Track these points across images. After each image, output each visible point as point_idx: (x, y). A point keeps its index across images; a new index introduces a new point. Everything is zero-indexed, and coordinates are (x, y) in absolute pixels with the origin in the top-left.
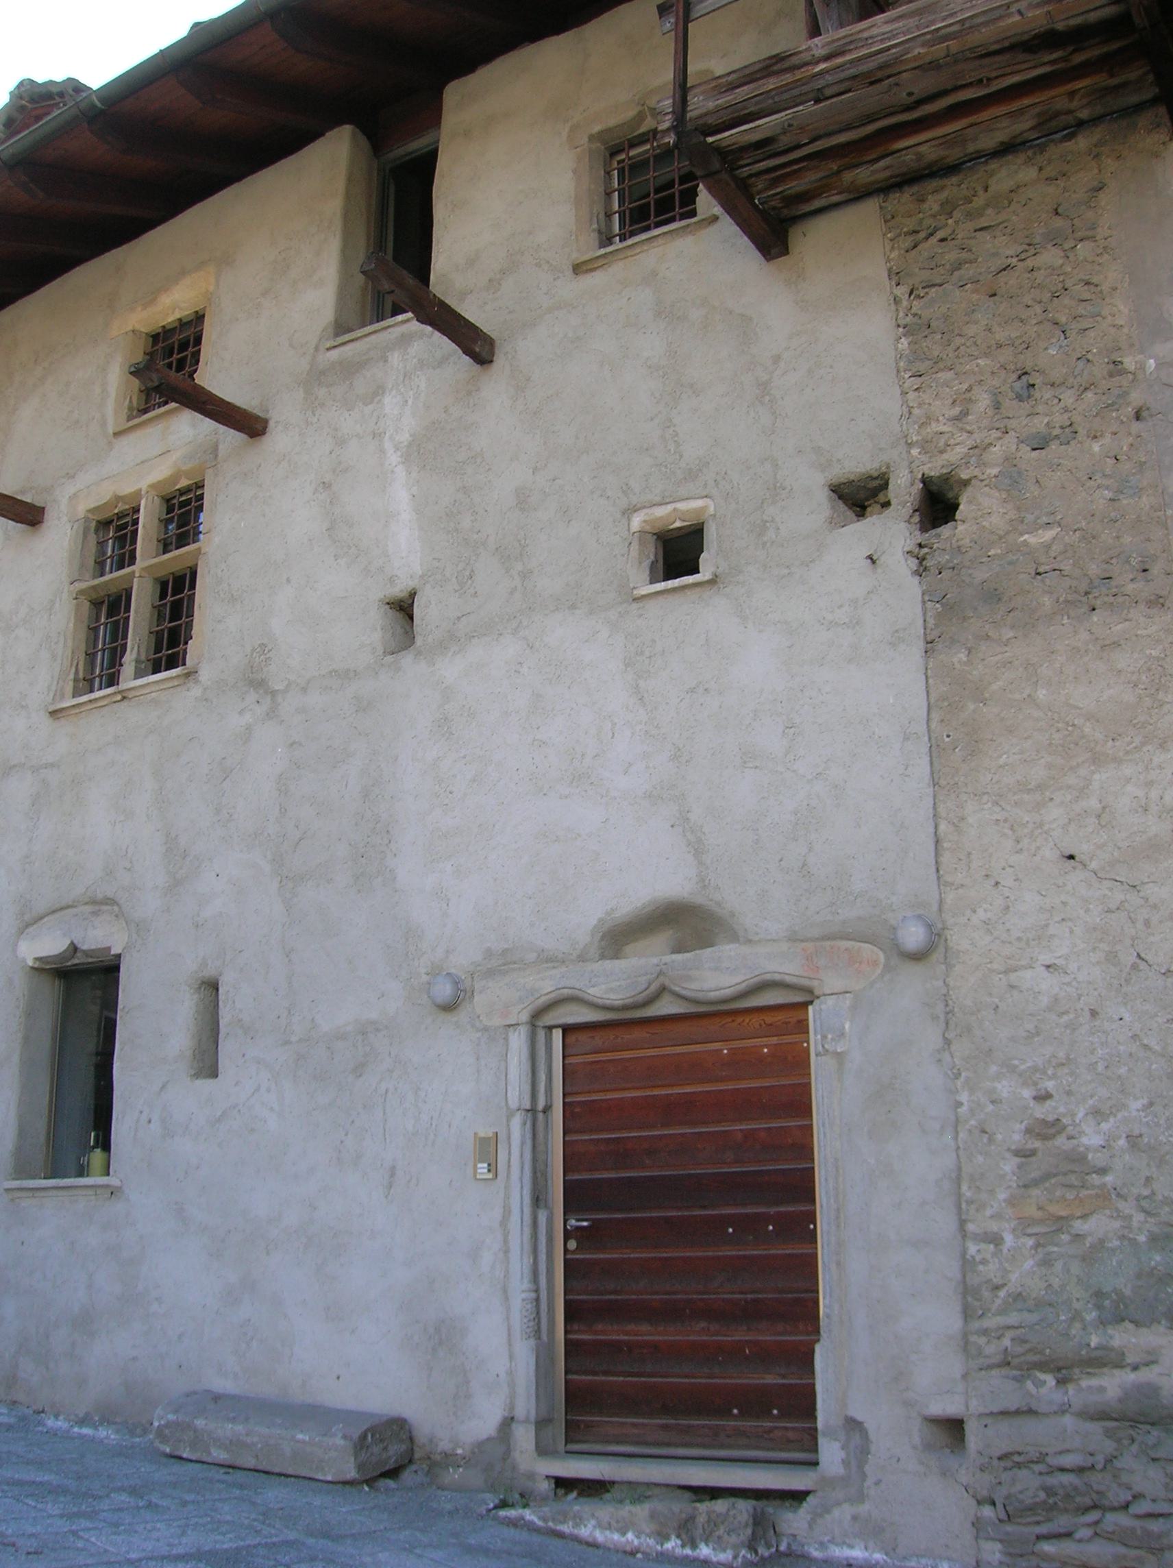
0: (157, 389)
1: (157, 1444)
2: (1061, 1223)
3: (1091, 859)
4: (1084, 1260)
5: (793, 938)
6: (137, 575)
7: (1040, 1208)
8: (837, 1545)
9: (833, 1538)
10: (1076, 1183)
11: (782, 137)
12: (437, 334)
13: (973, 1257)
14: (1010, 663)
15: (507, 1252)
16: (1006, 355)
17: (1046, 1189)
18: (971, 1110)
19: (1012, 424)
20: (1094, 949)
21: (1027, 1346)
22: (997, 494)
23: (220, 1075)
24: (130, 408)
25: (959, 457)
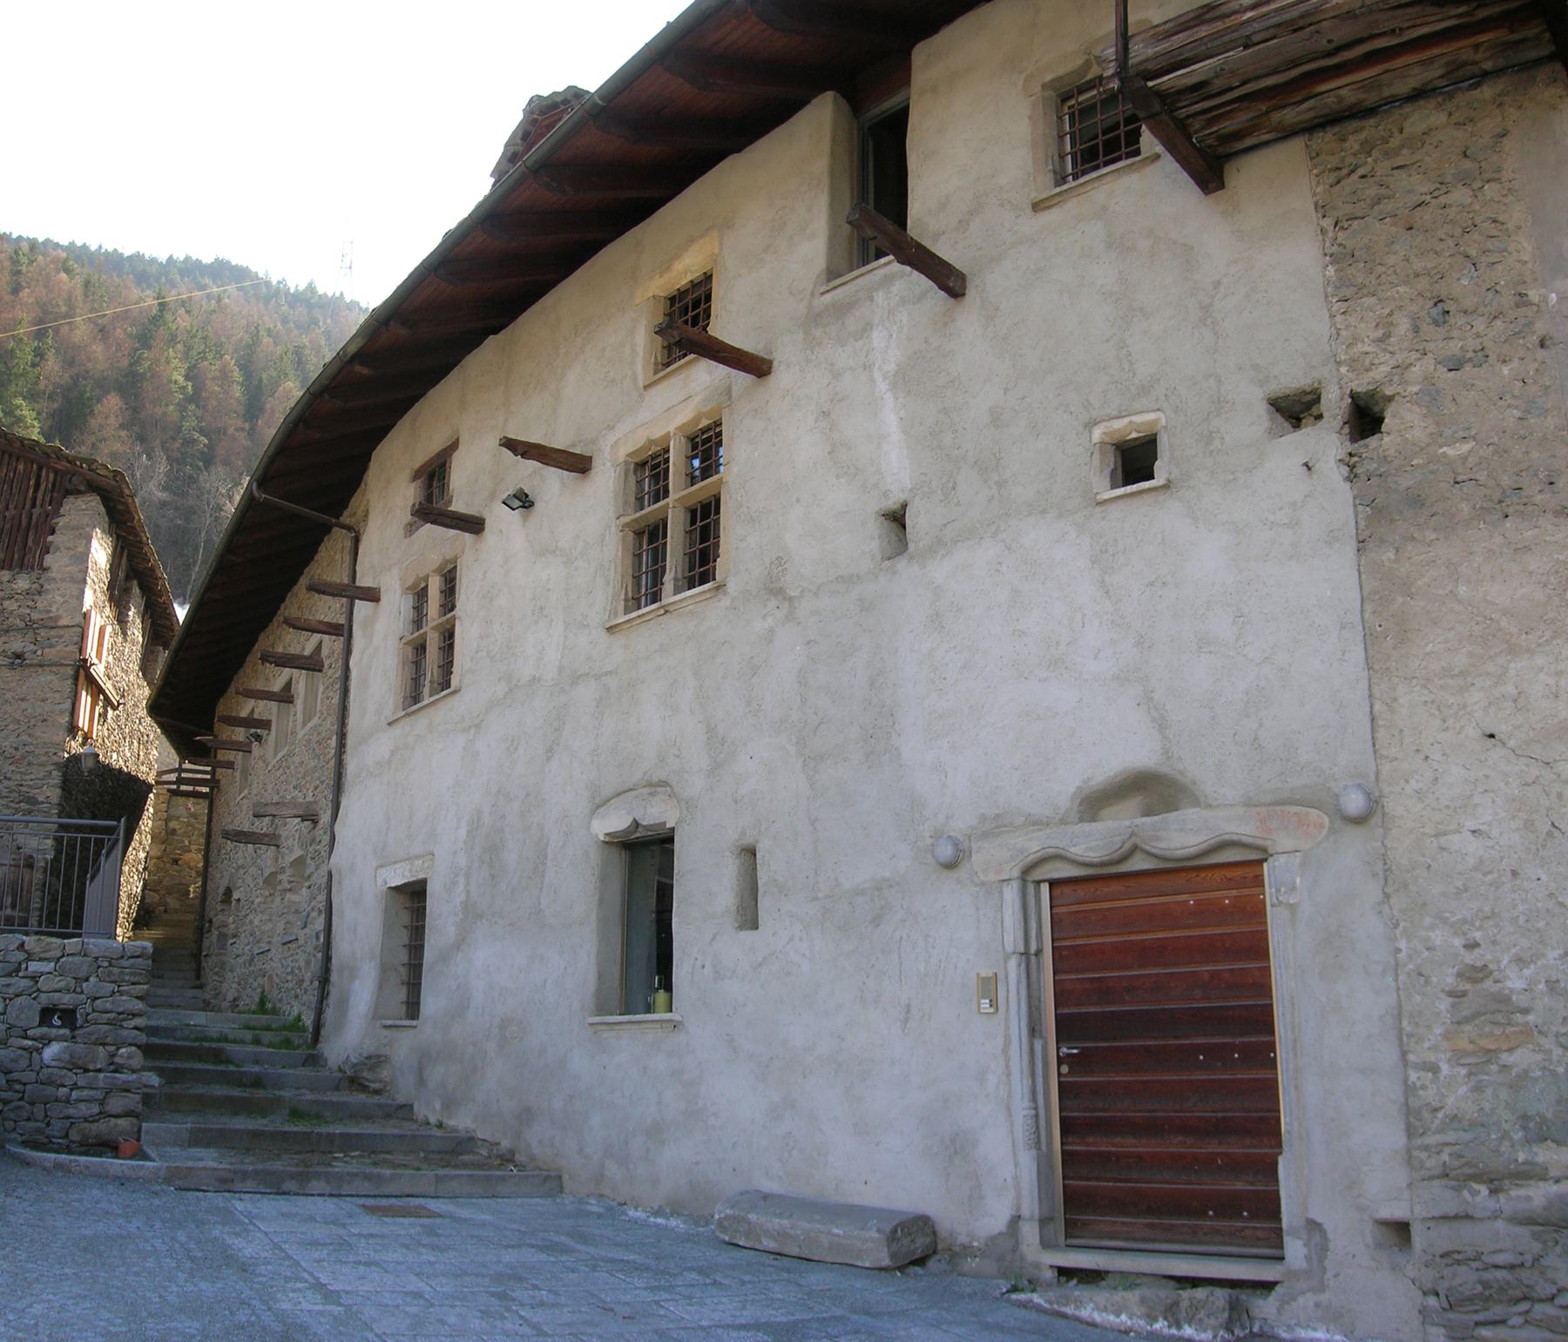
0: (679, 344)
1: (718, 1233)
2: (1490, 1055)
3: (1509, 738)
4: (1511, 1087)
5: (1248, 803)
7: (1471, 1042)
8: (1303, 1328)
9: (1299, 1322)
10: (1503, 1021)
11: (1216, 81)
12: (916, 273)
13: (1414, 1083)
14: (1433, 561)
15: (1009, 1075)
16: (1423, 284)
17: (1476, 1026)
18: (1410, 957)
19: (1430, 346)
20: (1514, 817)
21: (1463, 1160)
22: (1418, 410)
24: (656, 364)
25: (1383, 375)
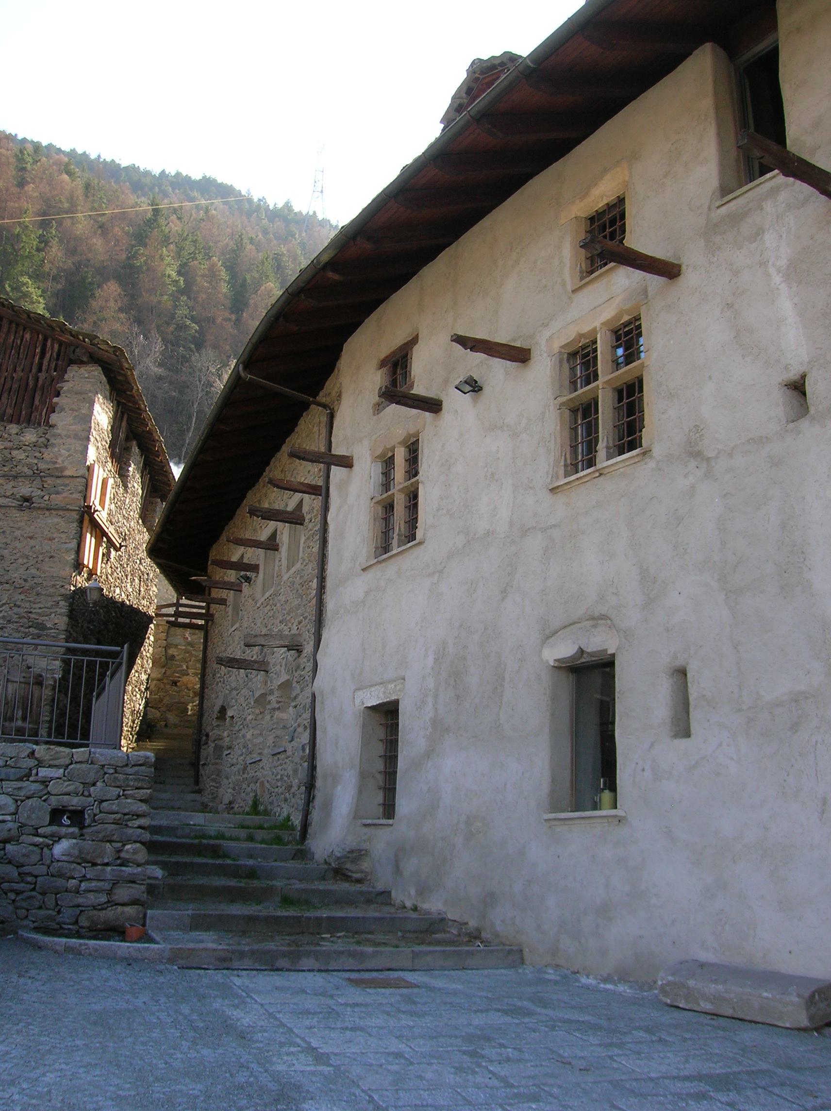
0: (601, 255)
6: (600, 387)
12: (798, 182)
23: (692, 736)
24: (581, 272)
